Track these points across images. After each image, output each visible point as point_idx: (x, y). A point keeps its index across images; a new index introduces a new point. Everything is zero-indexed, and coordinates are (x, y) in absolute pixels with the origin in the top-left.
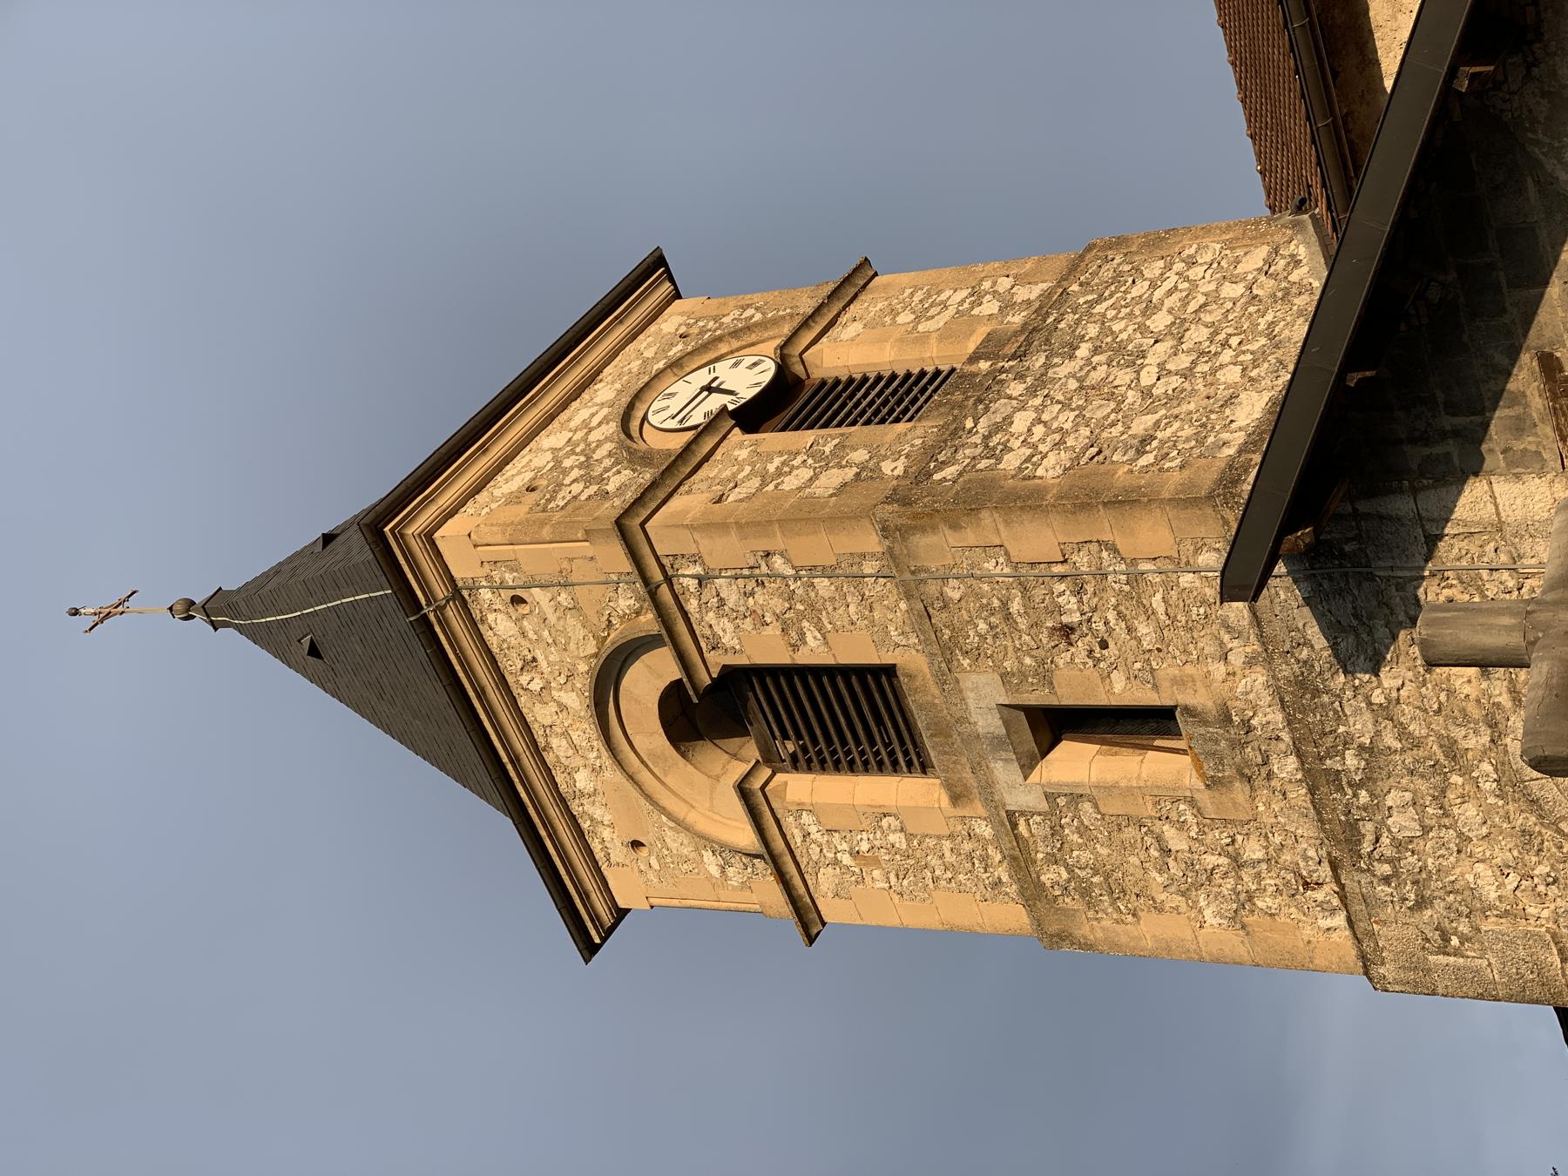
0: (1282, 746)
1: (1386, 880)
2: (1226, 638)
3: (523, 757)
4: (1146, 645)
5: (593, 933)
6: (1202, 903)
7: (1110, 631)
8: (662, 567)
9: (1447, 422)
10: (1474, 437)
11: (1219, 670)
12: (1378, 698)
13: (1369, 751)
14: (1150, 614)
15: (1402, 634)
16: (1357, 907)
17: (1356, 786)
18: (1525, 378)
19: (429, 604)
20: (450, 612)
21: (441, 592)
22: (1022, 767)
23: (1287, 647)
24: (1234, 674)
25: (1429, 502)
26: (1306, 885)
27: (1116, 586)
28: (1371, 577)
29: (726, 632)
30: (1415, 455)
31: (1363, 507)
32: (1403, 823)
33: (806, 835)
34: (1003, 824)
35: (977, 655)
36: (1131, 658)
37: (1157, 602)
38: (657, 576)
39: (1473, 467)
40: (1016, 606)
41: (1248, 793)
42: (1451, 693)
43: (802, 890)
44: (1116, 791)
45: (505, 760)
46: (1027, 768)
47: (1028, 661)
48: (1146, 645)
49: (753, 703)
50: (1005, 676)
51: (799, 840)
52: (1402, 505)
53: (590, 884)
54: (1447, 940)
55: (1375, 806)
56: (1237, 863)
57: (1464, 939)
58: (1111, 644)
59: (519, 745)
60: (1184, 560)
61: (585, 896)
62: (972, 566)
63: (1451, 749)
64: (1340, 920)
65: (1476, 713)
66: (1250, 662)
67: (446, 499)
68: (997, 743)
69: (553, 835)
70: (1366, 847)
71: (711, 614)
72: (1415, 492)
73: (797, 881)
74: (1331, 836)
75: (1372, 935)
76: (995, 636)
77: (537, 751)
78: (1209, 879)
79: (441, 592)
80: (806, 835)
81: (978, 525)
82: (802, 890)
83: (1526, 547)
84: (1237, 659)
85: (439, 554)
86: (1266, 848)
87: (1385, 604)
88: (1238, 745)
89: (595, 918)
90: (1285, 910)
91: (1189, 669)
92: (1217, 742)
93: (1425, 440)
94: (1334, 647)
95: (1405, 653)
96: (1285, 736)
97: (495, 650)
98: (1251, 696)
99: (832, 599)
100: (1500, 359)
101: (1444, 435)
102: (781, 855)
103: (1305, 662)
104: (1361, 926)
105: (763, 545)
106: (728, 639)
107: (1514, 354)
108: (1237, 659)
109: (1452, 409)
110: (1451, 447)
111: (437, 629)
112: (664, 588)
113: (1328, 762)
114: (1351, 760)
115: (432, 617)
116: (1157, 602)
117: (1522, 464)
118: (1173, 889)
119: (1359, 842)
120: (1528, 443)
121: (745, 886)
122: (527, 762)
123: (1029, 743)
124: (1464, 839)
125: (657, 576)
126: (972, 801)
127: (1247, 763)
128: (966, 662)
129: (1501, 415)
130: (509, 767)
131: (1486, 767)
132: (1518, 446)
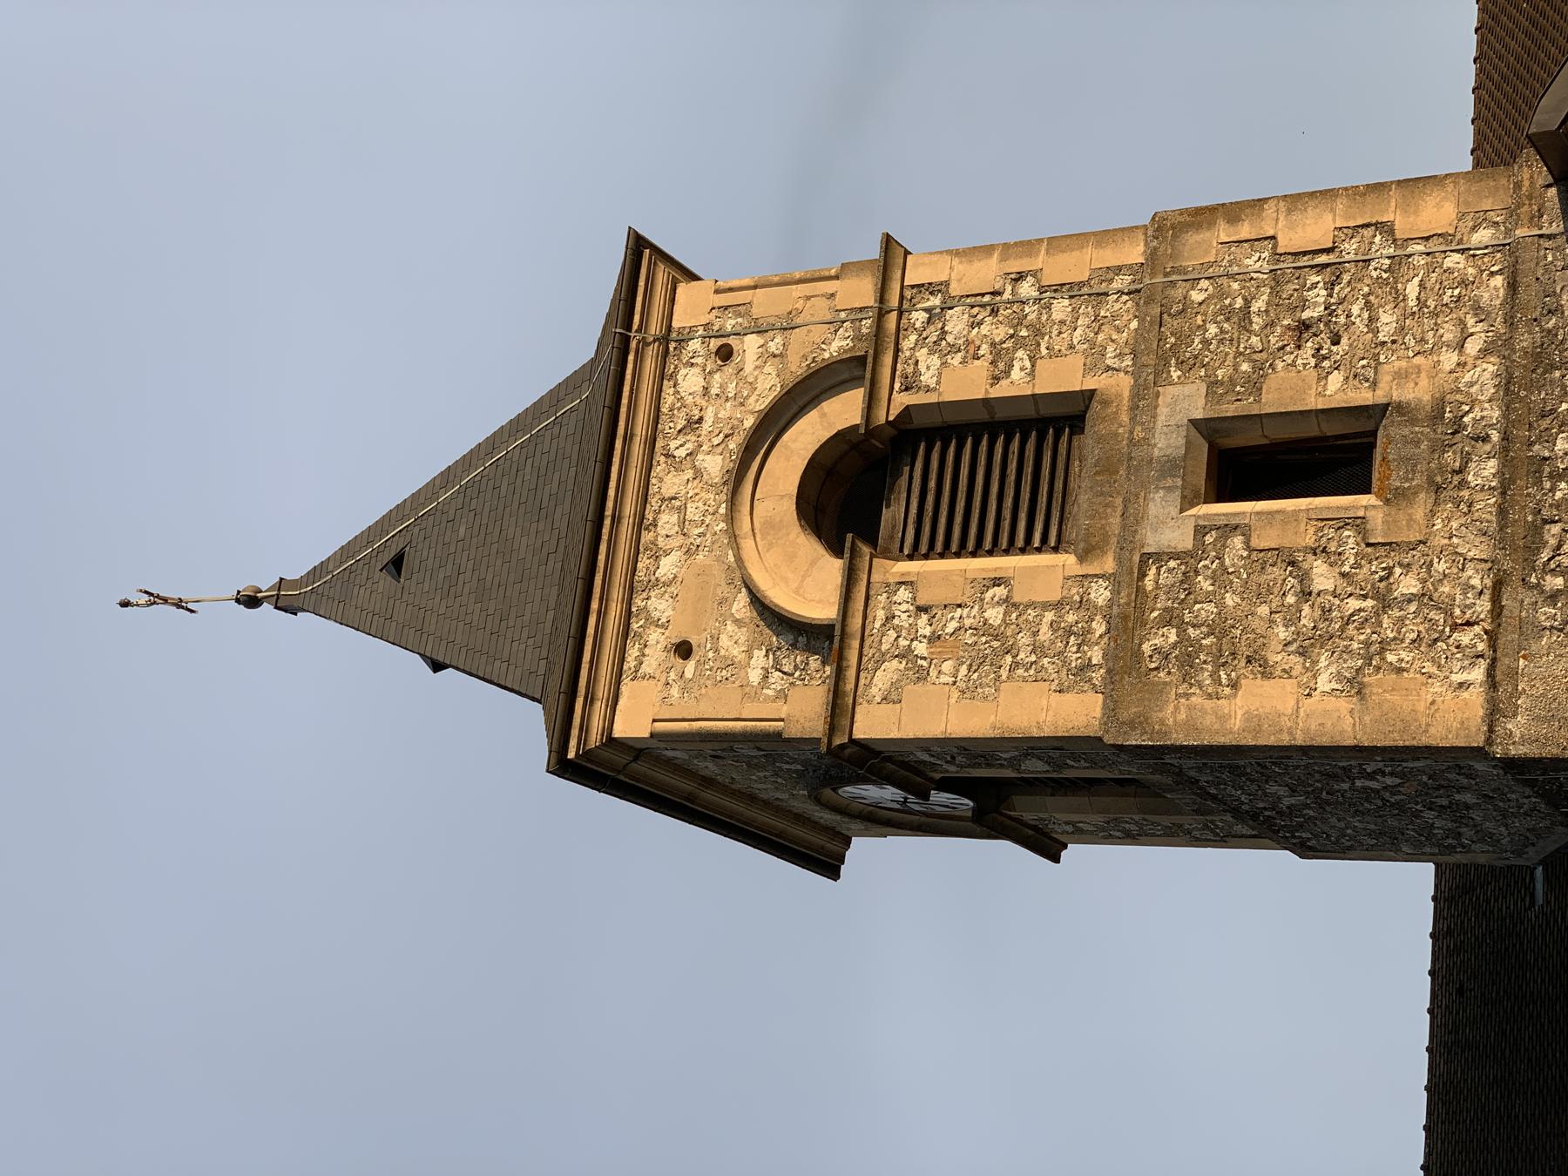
0: (1488, 447)
2: (1470, 321)
3: (625, 522)
4: (1381, 337)
5: (573, 743)
6: (1323, 662)
8: (902, 297)
11: (1449, 359)
14: (1399, 298)
16: (1508, 638)
19: (639, 330)
20: (651, 352)
21: (655, 328)
22: (1183, 497)
23: (1536, 314)
24: (1402, 641)
26: (1455, 627)
27: (1374, 274)
29: (928, 366)
33: (890, 618)
34: (1131, 573)
35: (1187, 366)
36: (1360, 353)
37: (1412, 290)
38: (894, 302)
41: (1429, 507)
43: (850, 686)
44: (1279, 517)
45: (608, 512)
46: (1188, 502)
47: (1245, 367)
48: (1381, 337)
49: (903, 482)
50: (1213, 384)
51: (877, 624)
53: (602, 690)
56: (1385, 602)
58: (1344, 341)
59: (629, 509)
60: (1458, 236)
61: (590, 699)
62: (1231, 263)
64: (1478, 674)
66: (1485, 352)
67: (640, 429)
68: (1170, 467)
69: (603, 614)
70: (1545, 556)
71: (925, 350)
73: (851, 674)
75: (1513, 674)
76: (1221, 341)
77: (640, 524)
78: (1342, 629)
79: (655, 328)
80: (890, 618)
81: (1259, 215)
82: (850, 686)
84: (1473, 346)
85: (673, 301)
86: (1424, 581)
88: (1440, 447)
89: (585, 728)
90: (1417, 664)
91: (1419, 360)
92: (1417, 443)
96: (1495, 436)
97: (664, 410)
98: (1473, 390)
99: (1062, 322)
102: (852, 636)
103: (1549, 331)
104: (1504, 662)
105: (1015, 266)
106: (927, 378)
108: (1473, 346)
111: (631, 358)
112: (894, 315)
113: (1537, 447)
115: (633, 344)
116: (1412, 290)
118: (1293, 648)
119: (1538, 551)
121: (782, 695)
123: (1200, 479)
125: (894, 302)
126: (1104, 553)
127: (1442, 469)
128: (1175, 374)
130: (607, 522)
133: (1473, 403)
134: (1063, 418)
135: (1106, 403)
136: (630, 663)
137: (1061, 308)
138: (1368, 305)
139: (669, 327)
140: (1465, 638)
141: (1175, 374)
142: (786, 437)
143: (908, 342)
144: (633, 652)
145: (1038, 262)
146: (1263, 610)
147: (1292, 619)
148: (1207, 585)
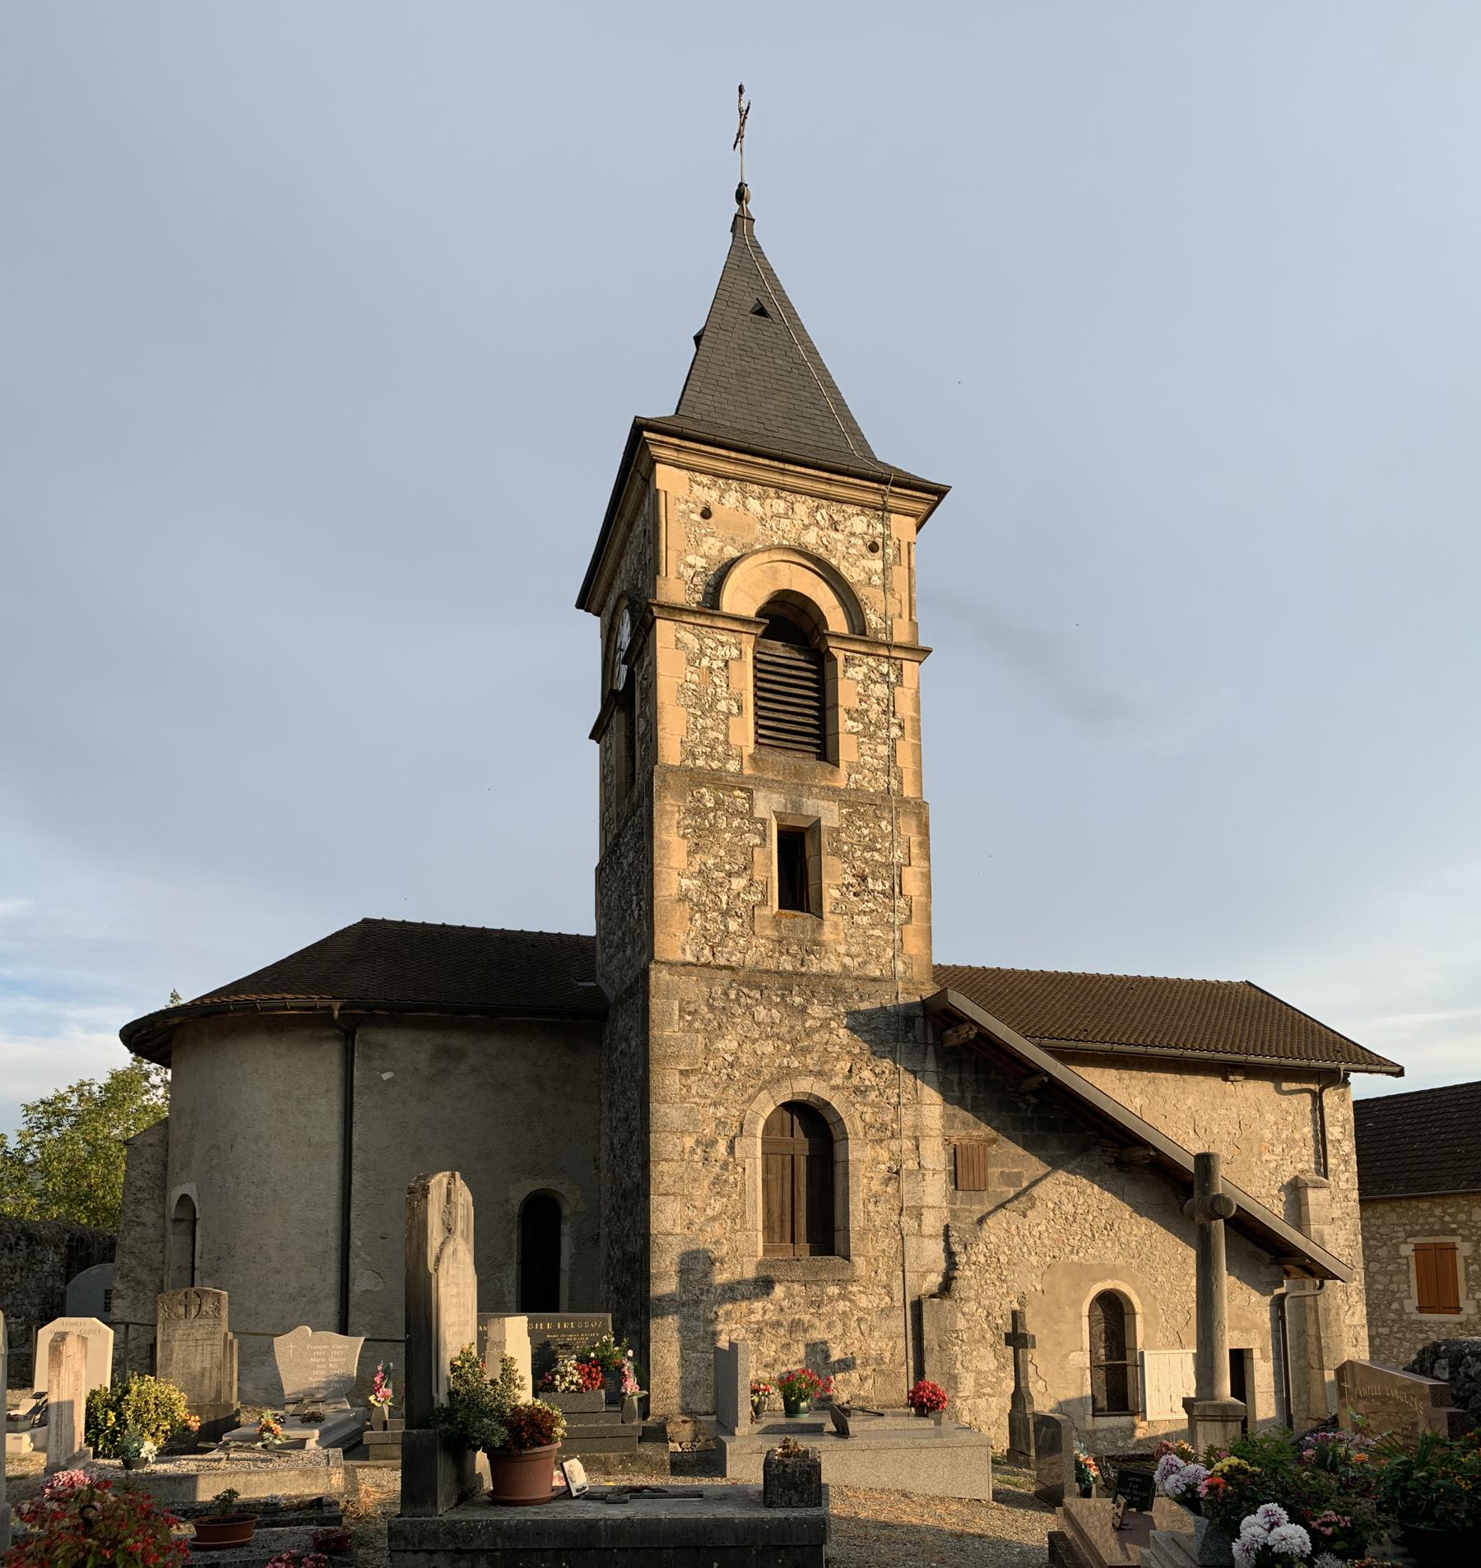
1: (726, 994)
7: (863, 901)
9: (969, 1095)
10: (960, 1103)
11: (842, 949)
12: (833, 1024)
13: (803, 1010)
14: (873, 926)
15: (866, 1046)
16: (707, 972)
17: (783, 997)
18: (984, 1131)
21: (892, 502)
25: (932, 1077)
28: (896, 1040)
30: (955, 1078)
31: (930, 1048)
32: (761, 1013)
37: (877, 932)
38: (894, 654)
39: (947, 1099)
40: (877, 856)
42: (837, 1059)
43: (685, 618)
45: (787, 466)
47: (846, 848)
50: (838, 831)
52: (931, 1065)
53: (684, 458)
54: (689, 1013)
55: (771, 1005)
56: (725, 914)
57: (690, 1023)
59: (789, 481)
63: (806, 1051)
64: (689, 958)
65: (828, 1067)
66: (844, 966)
68: (797, 806)
69: (728, 459)
72: (937, 1073)
73: (692, 619)
74: (752, 971)
75: (689, 974)
77: (780, 488)
82: (685, 618)
83: (910, 1111)
84: (847, 960)
87: (882, 1042)
89: (662, 444)
93: (961, 1084)
94: (859, 1012)
95: (858, 1046)
97: (844, 507)
100: (994, 1124)
101: (963, 1092)
105: (908, 726)
106: (851, 672)
107: (997, 1129)
108: (847, 960)
109: (974, 1099)
110: (957, 1094)
111: (876, 485)
114: (798, 1000)
116: (877, 932)
117: (948, 1120)
120: (957, 1124)
122: (776, 478)
124: (754, 1041)
127: (789, 944)
128: (844, 811)
129: (970, 1117)
130: (781, 465)
131: (796, 1064)
132: (957, 1121)
133: (820, 960)
134: (824, 748)
135: (832, 773)
136: (700, 477)
137: (883, 750)
138: (872, 911)
139: (890, 512)
140: (707, 951)
141: (844, 811)
142: (824, 584)
143: (871, 661)
144: (705, 479)
145: (909, 739)
146: (722, 853)
147: (717, 867)
148: (735, 824)
